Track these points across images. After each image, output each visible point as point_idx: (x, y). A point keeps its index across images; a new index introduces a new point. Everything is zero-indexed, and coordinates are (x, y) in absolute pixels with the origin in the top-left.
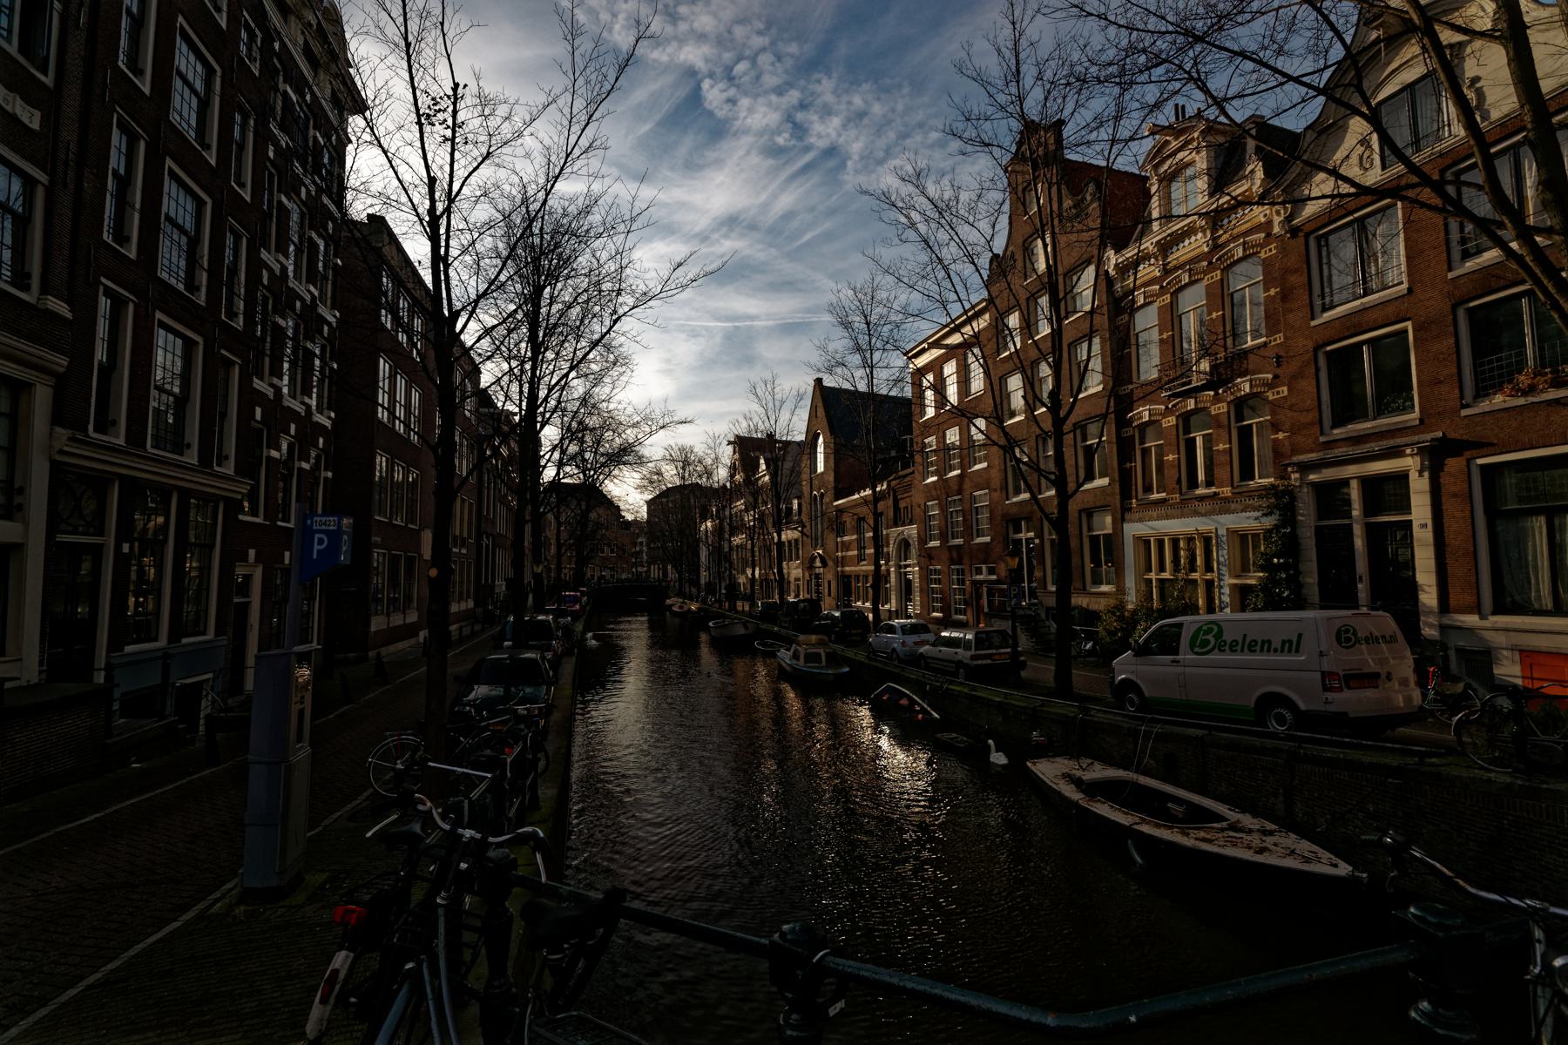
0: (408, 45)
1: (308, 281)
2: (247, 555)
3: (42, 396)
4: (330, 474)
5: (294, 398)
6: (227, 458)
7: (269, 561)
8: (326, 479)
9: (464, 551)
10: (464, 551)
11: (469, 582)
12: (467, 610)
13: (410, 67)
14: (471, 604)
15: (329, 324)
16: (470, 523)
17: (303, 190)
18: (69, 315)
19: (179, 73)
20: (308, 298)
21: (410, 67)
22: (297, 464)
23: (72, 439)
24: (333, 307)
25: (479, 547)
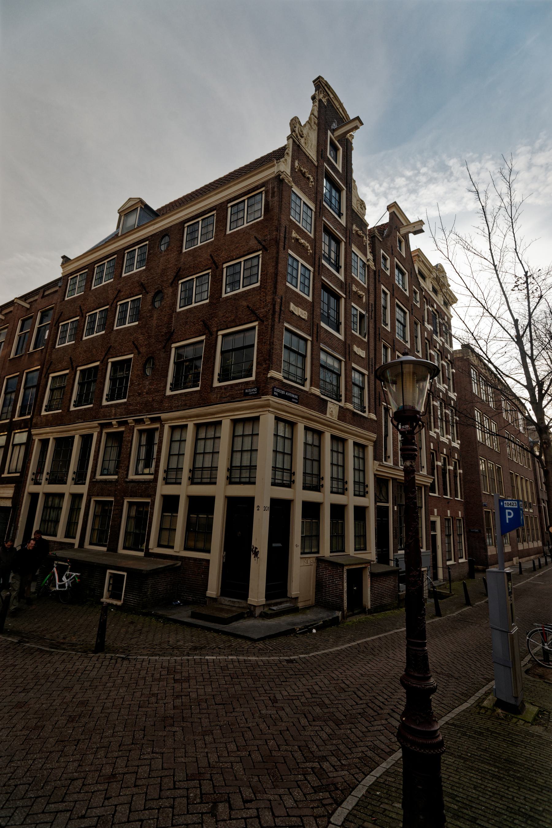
0: (495, 266)
1: (443, 383)
2: (434, 512)
3: (370, 450)
4: (461, 471)
5: (443, 436)
6: (389, 457)
7: (442, 514)
8: (460, 473)
9: (531, 511)
10: (531, 511)
11: (537, 529)
12: (538, 548)
13: (498, 275)
14: (540, 544)
15: (453, 400)
16: (532, 493)
17: (438, 345)
18: (376, 419)
19: (398, 320)
20: (444, 390)
21: (498, 275)
22: (448, 468)
23: (380, 465)
24: (454, 392)
25: (540, 508)
